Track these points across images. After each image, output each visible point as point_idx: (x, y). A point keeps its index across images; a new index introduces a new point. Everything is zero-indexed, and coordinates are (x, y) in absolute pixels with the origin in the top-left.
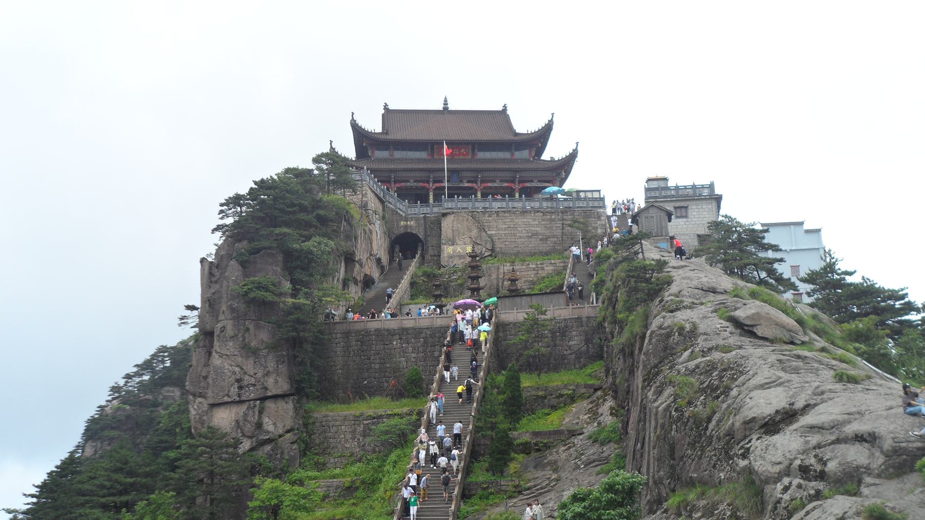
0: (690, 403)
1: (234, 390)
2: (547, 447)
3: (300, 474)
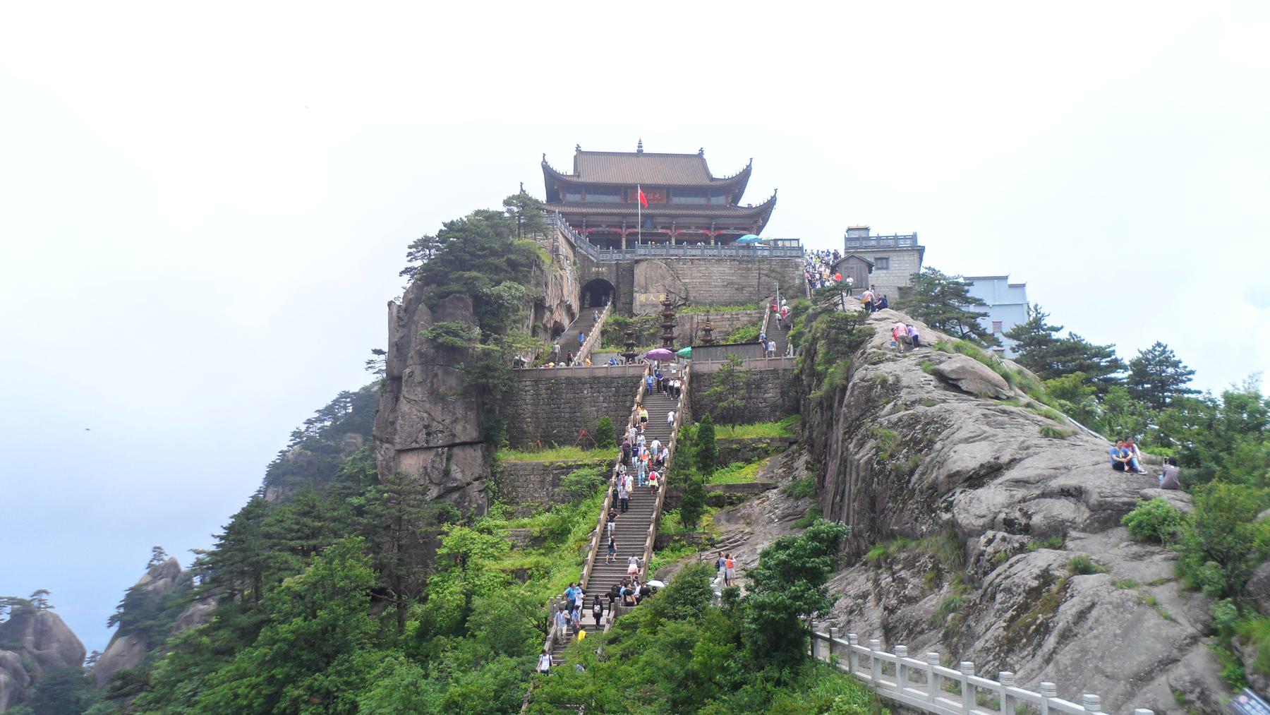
0: (892, 456)
1: (422, 436)
2: (741, 500)
3: (486, 522)
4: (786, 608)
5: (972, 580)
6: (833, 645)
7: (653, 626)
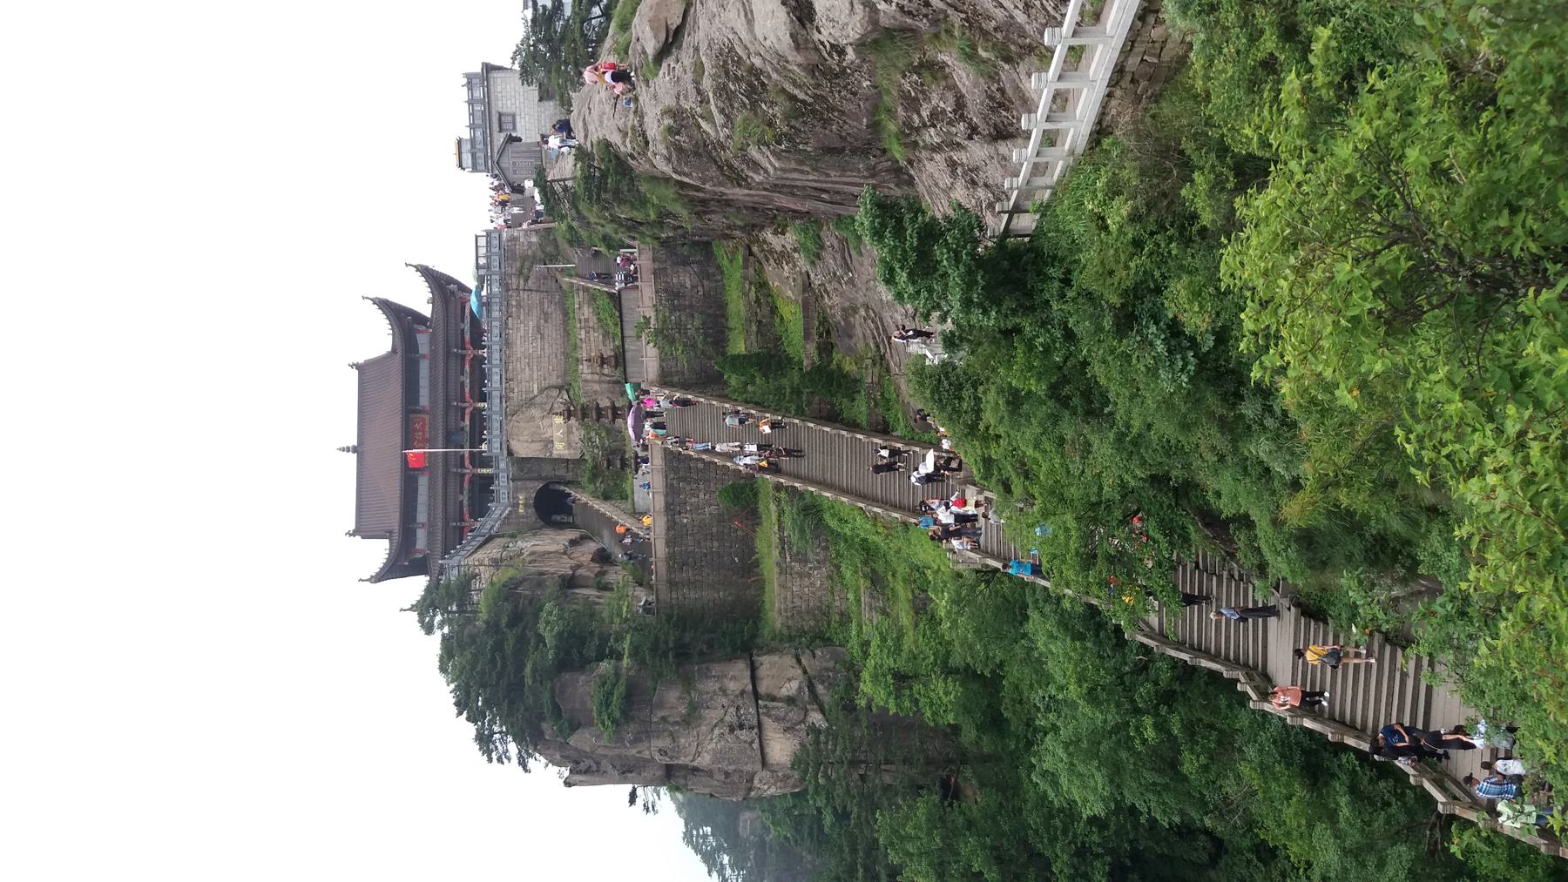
1: (744, 735)
2: (824, 321)
4: (970, 272)
5: (935, 22)
6: (1017, 209)
7: (988, 438)
